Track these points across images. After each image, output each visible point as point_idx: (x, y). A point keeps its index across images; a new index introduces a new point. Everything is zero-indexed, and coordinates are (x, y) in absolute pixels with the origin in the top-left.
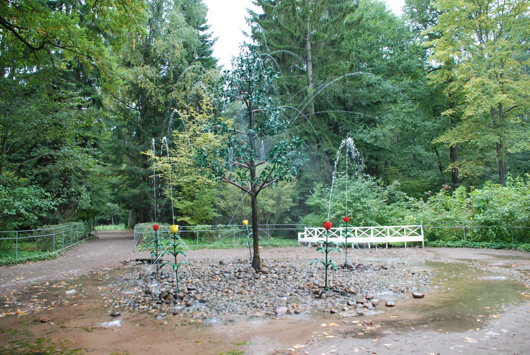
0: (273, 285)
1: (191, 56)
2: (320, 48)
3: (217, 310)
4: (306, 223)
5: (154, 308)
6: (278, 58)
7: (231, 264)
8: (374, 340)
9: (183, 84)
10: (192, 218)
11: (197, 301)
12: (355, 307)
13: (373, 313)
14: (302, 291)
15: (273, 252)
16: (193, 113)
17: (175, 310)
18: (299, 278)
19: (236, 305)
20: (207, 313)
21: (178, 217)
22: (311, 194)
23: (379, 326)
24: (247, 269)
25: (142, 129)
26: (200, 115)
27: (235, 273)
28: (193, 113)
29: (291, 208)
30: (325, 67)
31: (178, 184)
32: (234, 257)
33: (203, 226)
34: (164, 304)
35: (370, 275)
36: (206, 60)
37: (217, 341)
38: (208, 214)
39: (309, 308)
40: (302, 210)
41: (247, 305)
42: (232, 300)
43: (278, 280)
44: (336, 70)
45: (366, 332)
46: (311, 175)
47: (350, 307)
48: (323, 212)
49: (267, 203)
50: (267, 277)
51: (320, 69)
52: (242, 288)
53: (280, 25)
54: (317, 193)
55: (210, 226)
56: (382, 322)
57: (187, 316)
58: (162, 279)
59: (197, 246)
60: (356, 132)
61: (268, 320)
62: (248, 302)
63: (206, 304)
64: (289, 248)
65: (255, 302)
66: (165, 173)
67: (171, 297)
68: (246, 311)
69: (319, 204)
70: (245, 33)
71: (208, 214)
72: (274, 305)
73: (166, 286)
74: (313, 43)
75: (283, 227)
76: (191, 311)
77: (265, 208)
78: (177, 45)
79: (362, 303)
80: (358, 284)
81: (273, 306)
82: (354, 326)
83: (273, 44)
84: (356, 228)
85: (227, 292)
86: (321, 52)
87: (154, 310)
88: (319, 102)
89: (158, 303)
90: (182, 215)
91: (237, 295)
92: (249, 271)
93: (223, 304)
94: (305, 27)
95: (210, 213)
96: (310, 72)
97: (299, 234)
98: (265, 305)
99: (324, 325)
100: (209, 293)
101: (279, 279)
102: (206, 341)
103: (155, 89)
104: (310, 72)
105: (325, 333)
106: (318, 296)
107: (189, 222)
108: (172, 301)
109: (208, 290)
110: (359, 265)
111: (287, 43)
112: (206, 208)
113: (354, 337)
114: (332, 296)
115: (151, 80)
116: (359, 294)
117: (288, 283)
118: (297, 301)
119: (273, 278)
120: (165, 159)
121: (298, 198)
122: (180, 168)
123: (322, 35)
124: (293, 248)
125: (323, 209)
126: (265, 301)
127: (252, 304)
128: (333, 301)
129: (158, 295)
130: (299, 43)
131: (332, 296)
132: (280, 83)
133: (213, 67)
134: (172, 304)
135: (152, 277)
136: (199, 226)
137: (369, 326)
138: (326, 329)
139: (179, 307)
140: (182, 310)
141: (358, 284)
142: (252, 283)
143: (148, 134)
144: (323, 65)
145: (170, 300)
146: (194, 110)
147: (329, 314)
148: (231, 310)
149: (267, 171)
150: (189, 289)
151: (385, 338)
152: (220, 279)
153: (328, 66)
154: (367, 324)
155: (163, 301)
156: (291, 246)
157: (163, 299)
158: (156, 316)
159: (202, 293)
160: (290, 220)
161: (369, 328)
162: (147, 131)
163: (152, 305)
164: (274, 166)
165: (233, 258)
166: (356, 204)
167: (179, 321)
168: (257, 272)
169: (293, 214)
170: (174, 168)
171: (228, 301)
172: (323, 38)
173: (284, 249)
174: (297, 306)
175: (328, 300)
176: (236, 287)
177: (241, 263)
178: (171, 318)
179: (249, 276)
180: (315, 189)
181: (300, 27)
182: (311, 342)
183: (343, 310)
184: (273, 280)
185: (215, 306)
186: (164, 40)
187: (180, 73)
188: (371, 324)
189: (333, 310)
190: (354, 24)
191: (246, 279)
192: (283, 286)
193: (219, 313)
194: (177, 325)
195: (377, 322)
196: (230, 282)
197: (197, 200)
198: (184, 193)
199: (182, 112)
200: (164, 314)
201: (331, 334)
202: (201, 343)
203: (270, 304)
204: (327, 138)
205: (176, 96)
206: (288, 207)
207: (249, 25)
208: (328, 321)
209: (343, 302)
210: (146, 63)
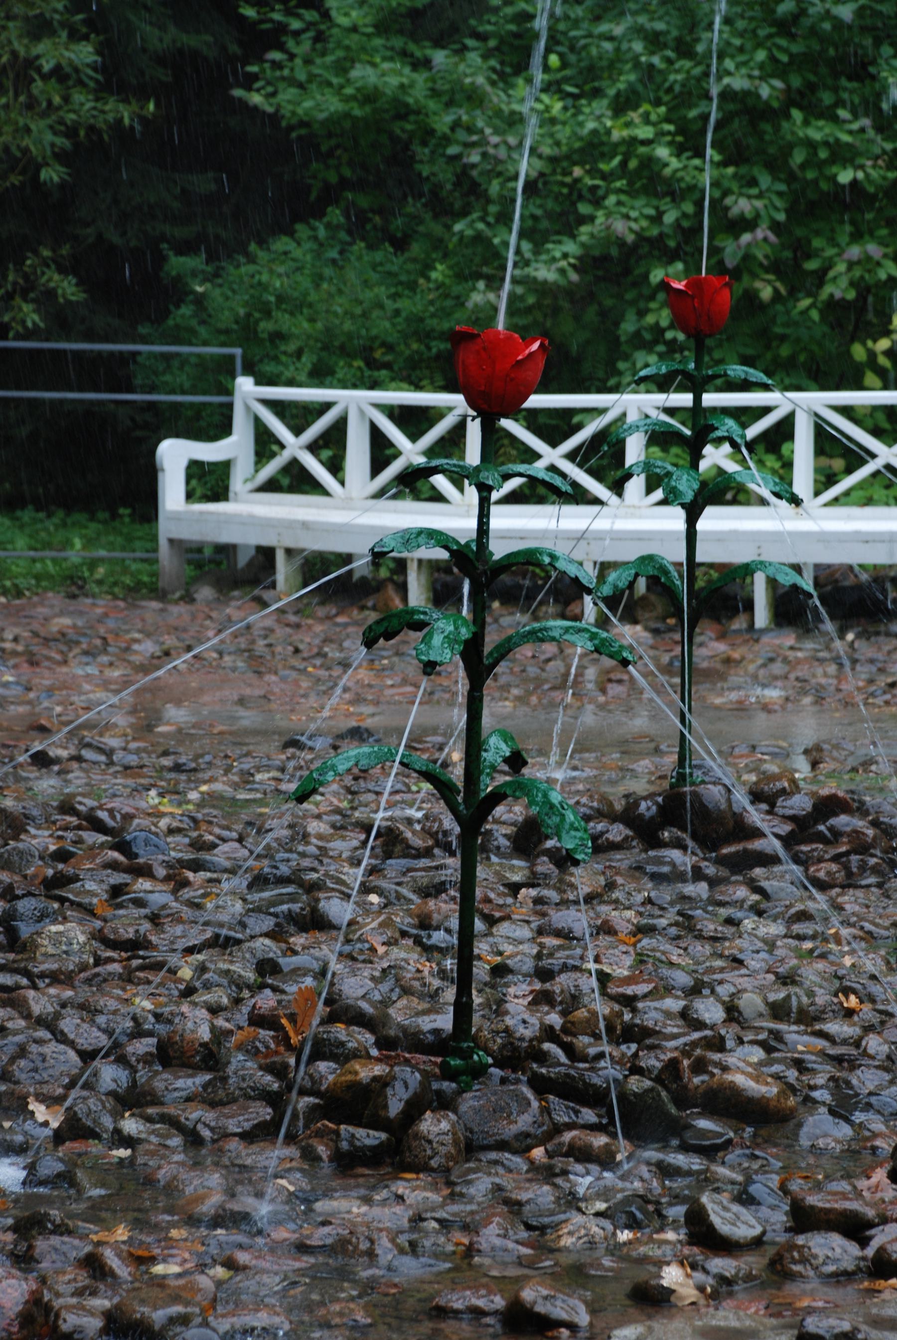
47: (721, 1265)
125: (445, 175)
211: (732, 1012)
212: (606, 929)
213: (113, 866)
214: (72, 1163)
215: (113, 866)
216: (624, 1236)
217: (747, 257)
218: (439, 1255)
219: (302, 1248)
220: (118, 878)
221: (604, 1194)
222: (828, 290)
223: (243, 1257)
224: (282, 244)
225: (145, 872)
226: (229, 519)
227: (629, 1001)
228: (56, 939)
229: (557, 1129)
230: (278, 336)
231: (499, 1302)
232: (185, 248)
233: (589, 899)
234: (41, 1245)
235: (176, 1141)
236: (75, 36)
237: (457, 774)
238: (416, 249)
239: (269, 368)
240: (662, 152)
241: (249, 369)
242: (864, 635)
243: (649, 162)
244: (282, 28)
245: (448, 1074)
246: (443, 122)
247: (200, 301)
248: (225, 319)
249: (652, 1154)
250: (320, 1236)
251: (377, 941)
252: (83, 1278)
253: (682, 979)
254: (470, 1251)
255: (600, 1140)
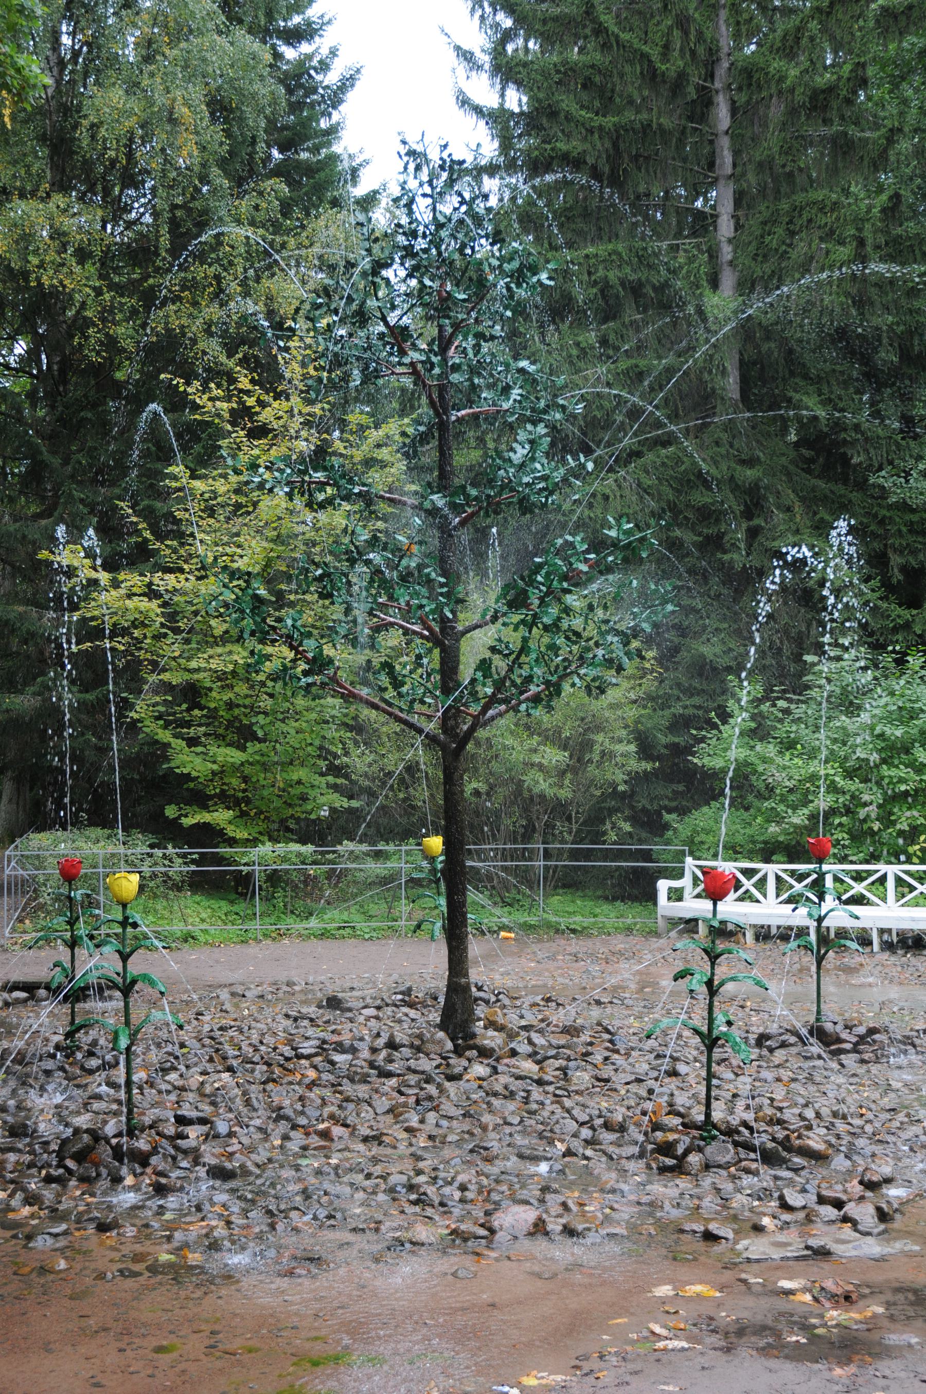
0: (511, 1106)
1: (244, 154)
2: (765, 125)
3: (269, 1212)
4: (690, 842)
5: (31, 1199)
6: (594, 168)
7: (371, 1012)
8: (838, 1371)
9: (211, 271)
10: (243, 814)
11: (202, 1171)
12: (809, 1219)
13: (872, 1247)
14: (612, 1137)
15: (553, 958)
16: (248, 393)
17: (110, 1207)
18: (618, 1079)
19: (348, 1190)
20: (229, 1223)
21: (188, 809)
22: (715, 726)
23: (880, 1310)
24: (420, 1036)
25: (46, 456)
26: (276, 404)
27: (374, 1050)
28: (248, 393)
29: (636, 779)
30: (785, 206)
31: (187, 676)
32: (395, 977)
33: (281, 848)
34: (73, 1183)
35: (908, 1077)
36: (310, 170)
37: (236, 1344)
38: (304, 798)
39: (626, 1212)
40: (681, 788)
41: (392, 1190)
42: (337, 1167)
43: (534, 1088)
44: (829, 219)
45: (820, 1331)
46: (718, 650)
47: (786, 1217)
48: (760, 796)
49: (536, 759)
50: (495, 1071)
51: (766, 214)
52: (389, 1119)
53: (600, 30)
54: (741, 719)
55: (310, 848)
56: (898, 1290)
57: (148, 1237)
58: (91, 1072)
59: (255, 925)
60: (908, 474)
61: (456, 1261)
62: (395, 1179)
63: (233, 1184)
64: (619, 943)
65: (422, 1179)
66: (136, 633)
67: (104, 1152)
68: (379, 1216)
69: (747, 764)
70: (467, 56)
71: (304, 798)
72: (495, 1197)
73: (96, 1105)
74: (742, 98)
75: (607, 855)
76: (168, 1216)
77: (528, 779)
78: (185, 110)
79: (838, 1204)
80: (844, 1117)
81: (487, 1200)
82: (781, 1304)
83: (574, 108)
84: (892, 870)
85: (325, 1135)
86: (772, 142)
87: (26, 1211)
88: (757, 346)
89: (49, 1180)
90: (201, 800)
91: (361, 1147)
92: (429, 1047)
93: (298, 1187)
94: (708, 35)
95: (312, 793)
96: (726, 228)
97: (663, 886)
98: (457, 1195)
99: (665, 1290)
100: (258, 1136)
101: (540, 1082)
102: (196, 1345)
103: (98, 292)
104: (726, 228)
105: (658, 1329)
106: (669, 1162)
107: (231, 831)
108: (104, 1172)
109: (257, 1122)
110: (872, 1031)
111: (631, 102)
112: (300, 773)
113: (764, 1351)
114: (726, 1166)
115: (82, 255)
116: (840, 1163)
117: (568, 1103)
118: (588, 1179)
119: (519, 1078)
120: (132, 579)
121: (663, 739)
122: (196, 613)
123: (777, 64)
124: (635, 940)
125: (762, 786)
126: (461, 1178)
127: (411, 1188)
128: (728, 1186)
129: (54, 1147)
130: (679, 101)
131: (726, 1166)
132: (601, 273)
133: (335, 203)
134: (104, 1184)
135: (49, 1065)
136: (266, 849)
137: (836, 1305)
138: (666, 1309)
139: (130, 1198)
140: (135, 1208)
141: (844, 1117)
142: (430, 1098)
143: (72, 477)
144: (777, 198)
145: (97, 1165)
146: (253, 381)
147: (701, 1246)
148: (322, 1214)
149: (496, 659)
150: (181, 1120)
151: (886, 1366)
152: (312, 1074)
153: (800, 198)
154: (833, 1297)
155: (69, 1171)
156: (629, 930)
157: (70, 1163)
158: (29, 1237)
159: (231, 1134)
160: (627, 827)
161: (835, 1313)
162: (66, 461)
163: (24, 1190)
164: (525, 640)
165: (390, 982)
166: (893, 772)
167: (116, 1255)
168: (458, 1051)
169: (643, 802)
170: (172, 615)
171: (319, 1172)
172: (782, 79)
173: (598, 946)
174: (582, 1205)
175: (707, 1181)
176: (367, 1113)
177: (411, 1005)
178: (86, 1245)
179: (425, 1064)
180: (731, 705)
181: (686, 33)
182: (594, 1364)
183: (758, 1229)
184: (515, 1085)
185: (265, 1194)
186: (133, 87)
187: (202, 226)
188: (847, 1298)
189: (713, 1227)
190: (915, 13)
191: (412, 1079)
192: (546, 1114)
193: (273, 1226)
194: (101, 1276)
195: (875, 1291)
196: (347, 1087)
197: (260, 741)
198: (213, 715)
199: (205, 389)
200: (64, 1227)
201: (677, 1333)
202: (175, 1355)
203: (480, 1192)
204: (790, 497)
205: (184, 321)
206: (620, 777)
207: (482, 18)
208: (683, 1272)
209: (762, 1195)
210: (63, 187)
211: (818, 1115)
212: (779, 1080)
213: (607, 1049)
214: (565, 1166)
215: (607, 1049)
216: (756, 1203)
217: (868, 816)
218: (688, 1208)
219: (639, 1203)
220: (608, 1054)
221: (750, 1187)
222: (898, 826)
223: (616, 1206)
224: (705, 809)
225: (617, 1052)
226: (683, 908)
227: (780, 1109)
228: (579, 1078)
229: (740, 1160)
230: (702, 843)
231: (702, 1228)
232: (669, 812)
233: (778, 1066)
234: (548, 1197)
235: (604, 1159)
236: (629, 742)
237: (705, 1029)
238: (752, 811)
239: (697, 854)
240: (837, 779)
241: (691, 853)
242: (914, 955)
243: (833, 782)
244: (705, 737)
245: (702, 1138)
246: (760, 769)
247: (675, 829)
248: (683, 836)
249: (773, 1172)
250: (645, 1199)
251: (693, 1082)
252: (560, 1210)
253: (801, 1101)
254: (698, 1207)
255: (754, 1166)
